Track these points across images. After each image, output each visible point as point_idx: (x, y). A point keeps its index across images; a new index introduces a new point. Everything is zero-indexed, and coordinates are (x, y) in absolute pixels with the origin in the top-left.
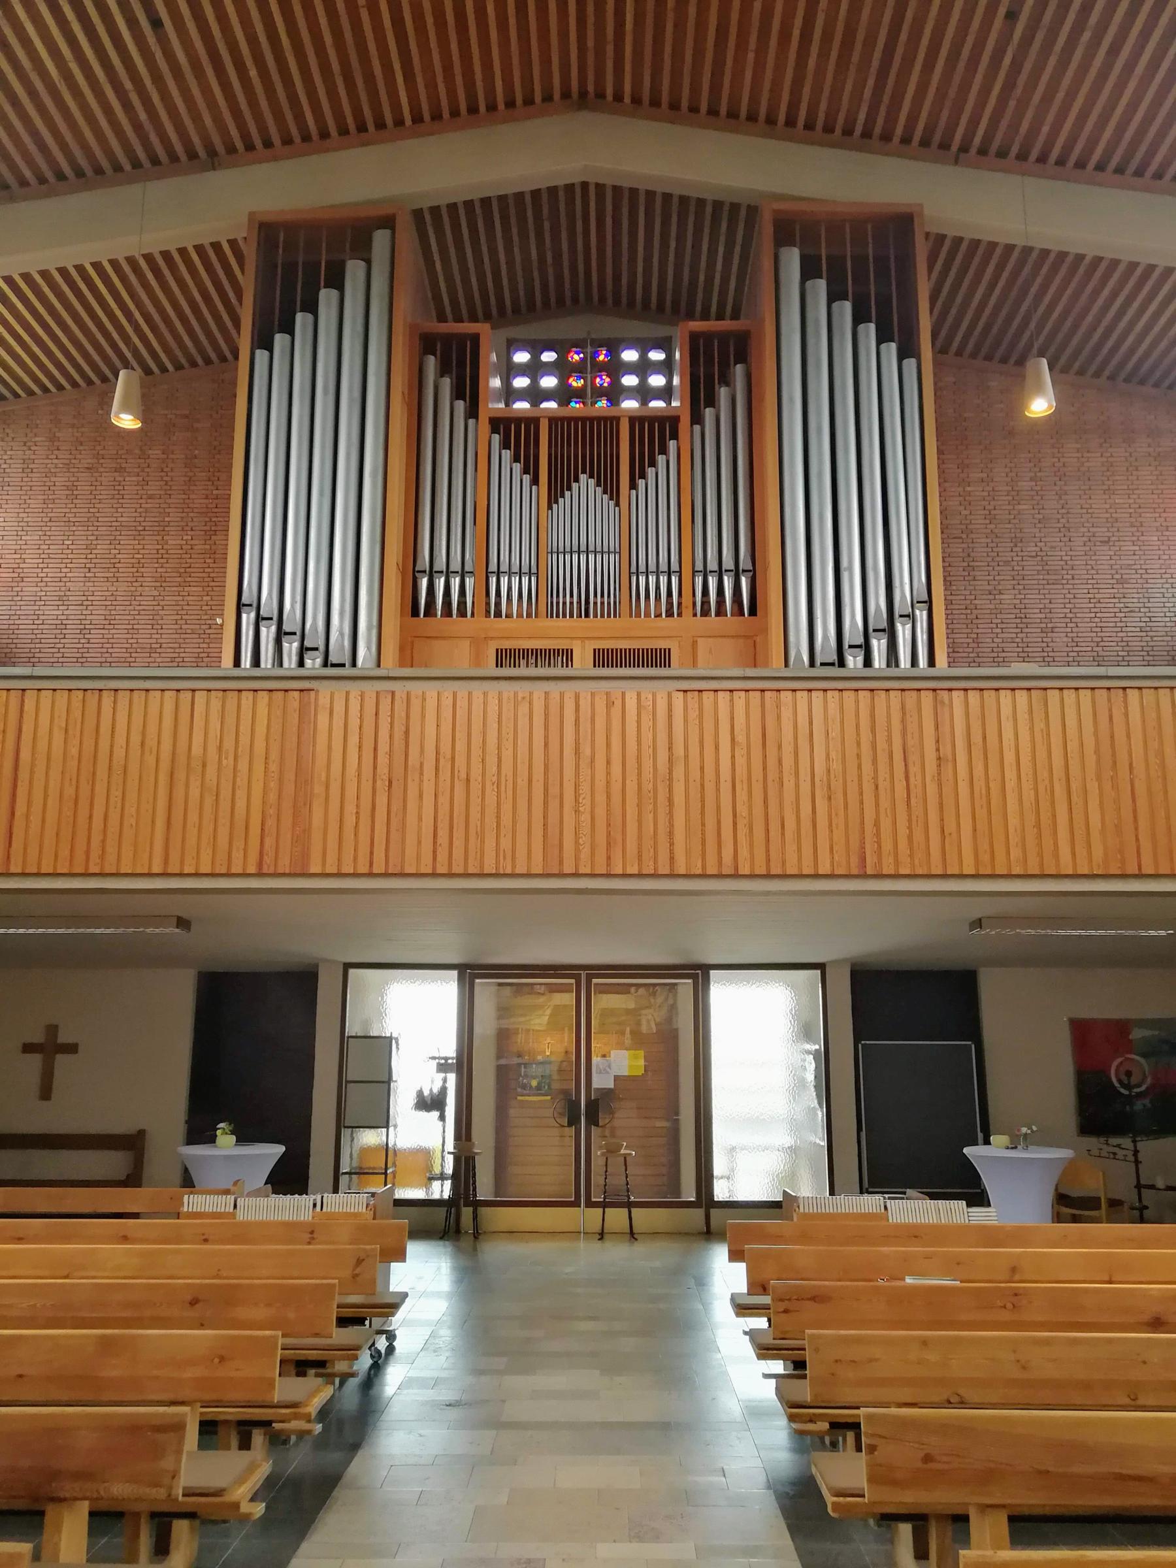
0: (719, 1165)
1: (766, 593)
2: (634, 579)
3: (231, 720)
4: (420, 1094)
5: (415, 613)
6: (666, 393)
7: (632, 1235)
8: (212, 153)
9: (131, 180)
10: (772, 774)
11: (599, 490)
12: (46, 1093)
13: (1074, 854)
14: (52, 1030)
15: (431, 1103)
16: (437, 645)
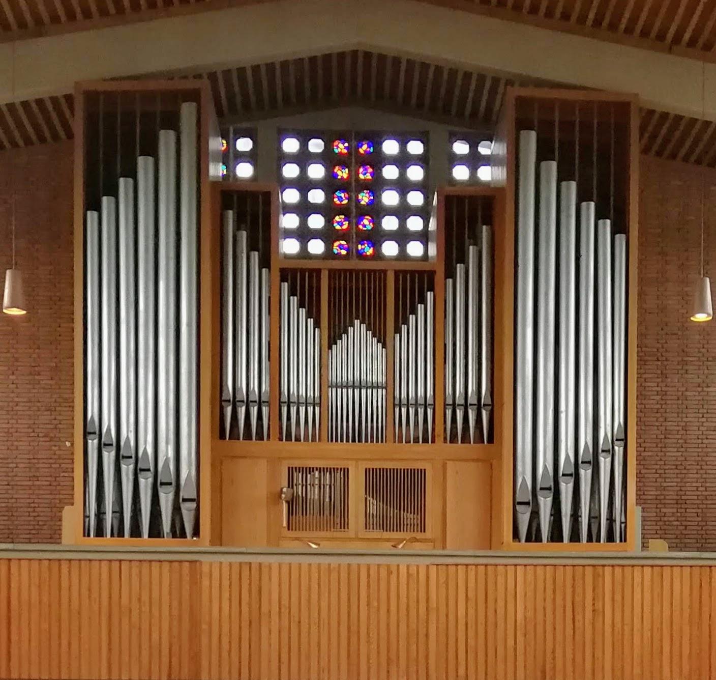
0: (195, 113)
1: (501, 422)
2: (397, 410)
5: (222, 436)
11: (370, 333)
13: (671, 671)
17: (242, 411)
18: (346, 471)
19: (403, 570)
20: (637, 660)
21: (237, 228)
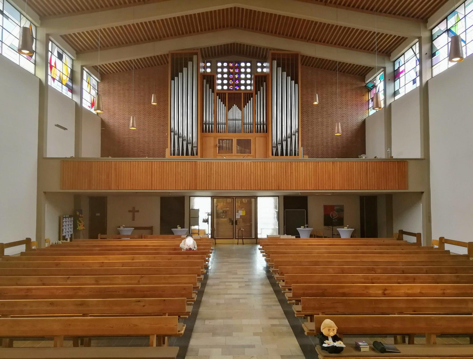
0: (259, 232)
3: (184, 166)
4: (204, 220)
5: (203, 132)
6: (250, 85)
7: (243, 244)
8: (160, 37)
9: (144, 43)
14: (134, 208)
15: (206, 221)
18: (232, 140)
20: (301, 184)
21: (207, 84)
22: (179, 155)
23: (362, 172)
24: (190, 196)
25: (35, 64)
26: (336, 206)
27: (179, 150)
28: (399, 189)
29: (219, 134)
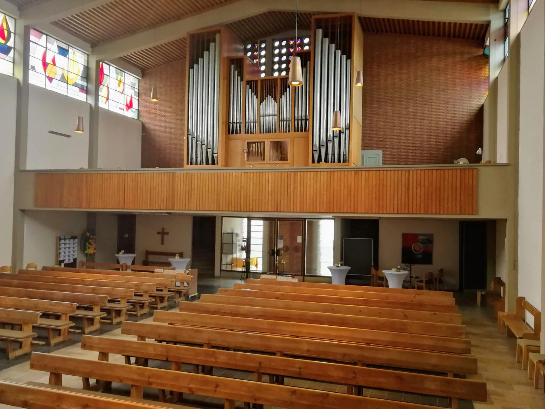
2: (296, 122)
5: (229, 133)
10: (261, 190)
12: (163, 243)
14: (163, 229)
16: (234, 141)
17: (235, 125)
18: (264, 142)
19: (234, 174)
20: (308, 204)
21: (235, 70)
22: (334, 162)
23: (400, 186)
24: (223, 217)
25: (14, 63)
26: (422, 235)
27: (333, 154)
28: (461, 214)
29: (249, 135)
